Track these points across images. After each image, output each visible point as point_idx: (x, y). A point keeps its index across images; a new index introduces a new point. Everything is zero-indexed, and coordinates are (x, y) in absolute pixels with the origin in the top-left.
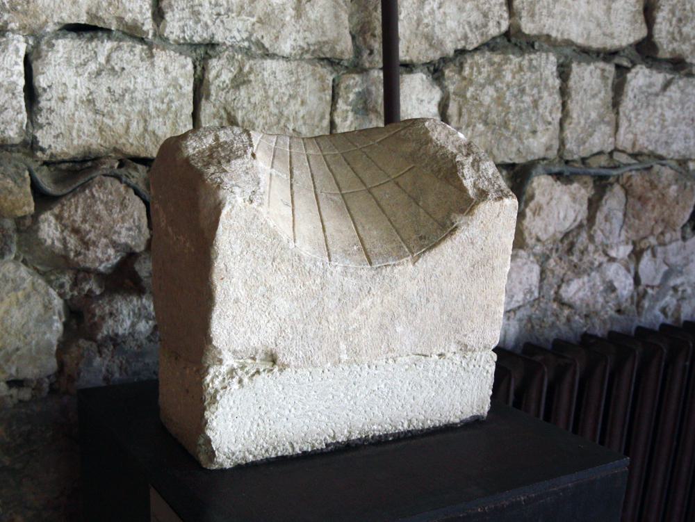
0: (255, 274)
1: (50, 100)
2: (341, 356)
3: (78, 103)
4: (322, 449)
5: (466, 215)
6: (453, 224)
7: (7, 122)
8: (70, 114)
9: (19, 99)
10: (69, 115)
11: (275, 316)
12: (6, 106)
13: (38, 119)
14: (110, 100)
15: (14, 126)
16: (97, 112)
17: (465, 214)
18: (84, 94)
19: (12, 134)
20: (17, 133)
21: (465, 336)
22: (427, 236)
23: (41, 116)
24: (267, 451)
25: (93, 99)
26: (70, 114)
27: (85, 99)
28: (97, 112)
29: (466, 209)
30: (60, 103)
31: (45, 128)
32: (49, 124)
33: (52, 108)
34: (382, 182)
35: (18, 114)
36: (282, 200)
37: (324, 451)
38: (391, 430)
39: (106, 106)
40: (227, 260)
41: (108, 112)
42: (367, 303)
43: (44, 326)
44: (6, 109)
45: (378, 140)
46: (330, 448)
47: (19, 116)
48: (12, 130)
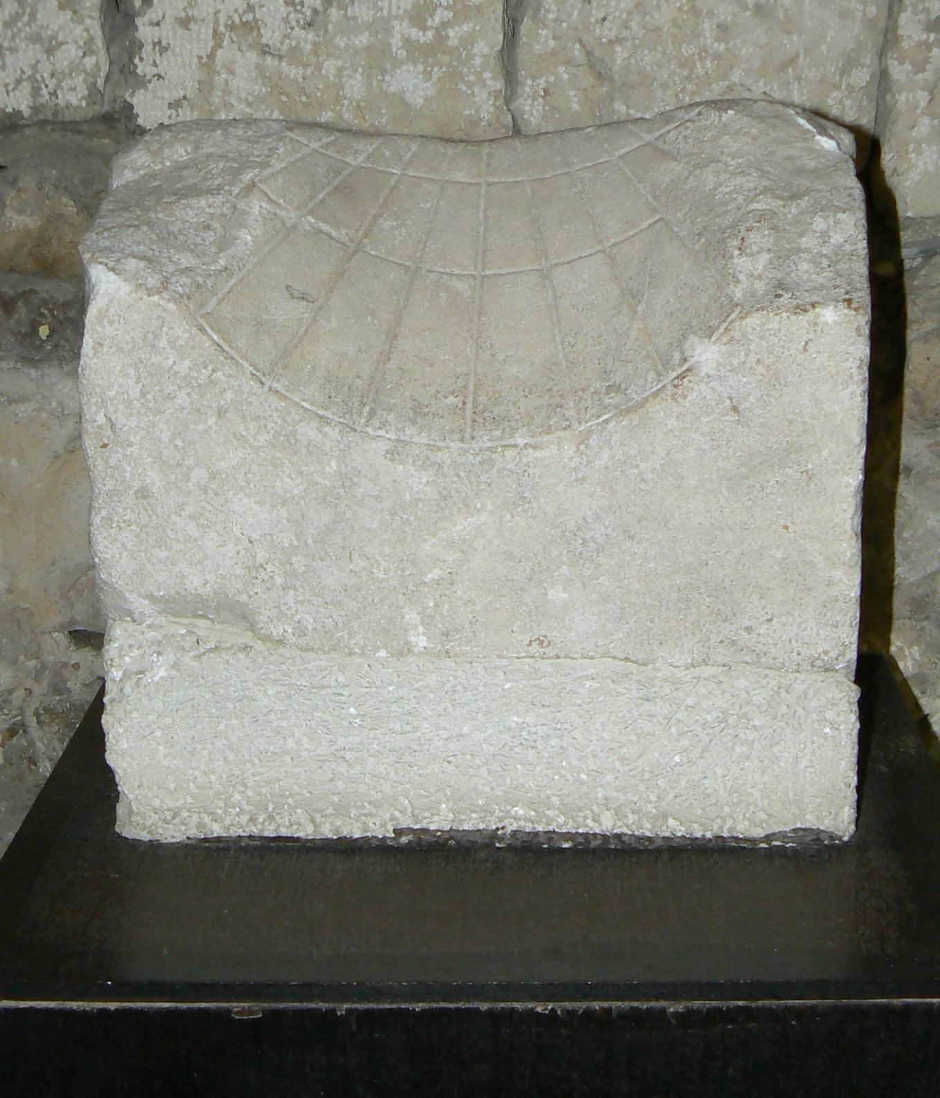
0: (179, 443)
1: (158, 24)
2: (412, 639)
3: (222, 29)
4: (385, 838)
5: (715, 342)
6: (685, 360)
7: (63, 73)
8: (203, 54)
9: (88, 21)
10: (200, 58)
11: (239, 534)
12: (60, 38)
13: (136, 67)
14: (294, 23)
15: (79, 80)
16: (265, 51)
17: (713, 339)
18: (236, 11)
19: (74, 100)
20: (83, 98)
21: (749, 629)
22: (623, 386)
23: (141, 59)
24: (252, 820)
25: (256, 20)
26: (203, 54)
27: (237, 21)
28: (265, 51)
29: (718, 327)
30: (180, 32)
31: (150, 86)
32: (159, 77)
33: (164, 43)
34: (584, 254)
35: (85, 55)
36: (287, 287)
37: (389, 842)
38: (562, 823)
39: (286, 36)
40: (111, 409)
41: (291, 49)
42: (461, 526)
43: (780, 556)
44: (61, 44)
45: (622, 151)
46: (404, 840)
47: (87, 59)
48: (74, 89)
